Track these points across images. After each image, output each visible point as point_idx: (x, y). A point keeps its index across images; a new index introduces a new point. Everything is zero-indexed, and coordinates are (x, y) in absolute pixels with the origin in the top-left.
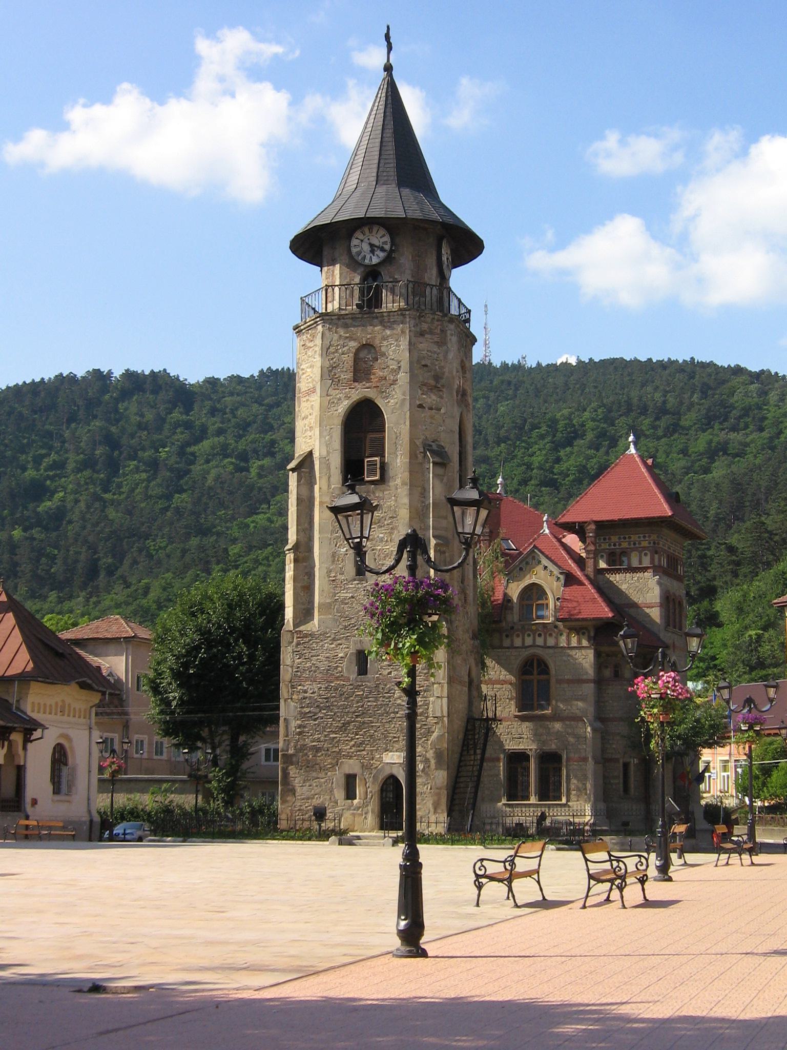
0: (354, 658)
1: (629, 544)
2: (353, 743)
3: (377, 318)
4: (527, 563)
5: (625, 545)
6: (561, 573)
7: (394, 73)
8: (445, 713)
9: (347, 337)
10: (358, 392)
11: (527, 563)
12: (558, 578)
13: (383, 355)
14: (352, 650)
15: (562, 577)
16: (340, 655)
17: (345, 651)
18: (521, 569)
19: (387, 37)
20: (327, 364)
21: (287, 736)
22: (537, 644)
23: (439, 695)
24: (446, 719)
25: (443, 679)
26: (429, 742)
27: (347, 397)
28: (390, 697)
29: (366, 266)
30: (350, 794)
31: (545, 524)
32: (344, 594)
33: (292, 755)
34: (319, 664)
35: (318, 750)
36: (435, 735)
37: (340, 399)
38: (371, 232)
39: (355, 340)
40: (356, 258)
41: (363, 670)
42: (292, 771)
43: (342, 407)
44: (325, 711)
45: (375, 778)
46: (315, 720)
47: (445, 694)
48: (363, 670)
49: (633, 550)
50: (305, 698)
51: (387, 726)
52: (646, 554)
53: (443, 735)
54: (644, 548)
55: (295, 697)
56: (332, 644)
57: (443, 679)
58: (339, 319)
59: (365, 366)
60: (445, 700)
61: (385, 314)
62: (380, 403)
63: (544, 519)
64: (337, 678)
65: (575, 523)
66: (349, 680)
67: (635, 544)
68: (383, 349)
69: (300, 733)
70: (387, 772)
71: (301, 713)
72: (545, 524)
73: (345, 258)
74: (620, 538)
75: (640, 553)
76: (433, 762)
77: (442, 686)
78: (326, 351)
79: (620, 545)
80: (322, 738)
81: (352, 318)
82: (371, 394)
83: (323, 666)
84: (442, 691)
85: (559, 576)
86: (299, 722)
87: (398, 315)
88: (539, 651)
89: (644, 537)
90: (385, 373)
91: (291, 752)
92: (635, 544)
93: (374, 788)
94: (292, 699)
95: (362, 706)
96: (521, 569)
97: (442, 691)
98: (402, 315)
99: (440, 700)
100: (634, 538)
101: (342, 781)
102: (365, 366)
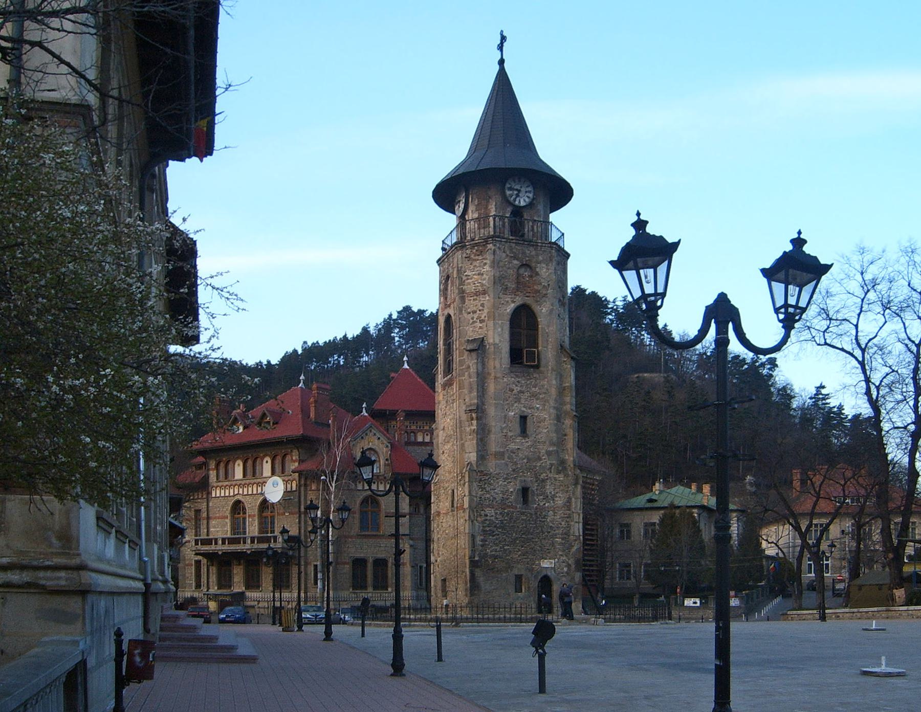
0: (520, 492)
1: (417, 427)
3: (533, 245)
4: (366, 434)
5: (414, 427)
6: (389, 443)
7: (505, 65)
8: (581, 534)
9: (511, 257)
10: (519, 301)
11: (366, 434)
12: (387, 446)
13: (537, 274)
15: (389, 446)
16: (511, 490)
18: (362, 438)
20: (498, 274)
21: (474, 547)
22: (380, 489)
24: (581, 537)
25: (580, 510)
27: (513, 302)
29: (517, 207)
30: (518, 589)
31: (364, 409)
32: (512, 446)
35: (496, 557)
36: (575, 548)
37: (508, 302)
38: (520, 181)
39: (517, 260)
42: (478, 573)
44: (500, 530)
45: (536, 577)
46: (493, 536)
47: (581, 520)
50: (487, 520)
51: (543, 541)
52: (427, 435)
54: (426, 431)
55: (479, 519)
56: (505, 481)
57: (580, 510)
58: (506, 242)
60: (581, 525)
61: (539, 244)
62: (536, 308)
63: (364, 406)
64: (509, 507)
65: (386, 410)
66: (516, 508)
67: (420, 427)
69: (482, 546)
71: (484, 531)
72: (364, 409)
73: (499, 198)
75: (424, 433)
76: (573, 566)
77: (579, 515)
82: (529, 301)
83: (499, 497)
84: (579, 518)
85: (388, 444)
86: (482, 537)
87: (548, 247)
88: (240, 498)
89: (427, 423)
90: (540, 287)
91: (477, 558)
92: (420, 427)
93: (535, 584)
94: (477, 520)
96: (362, 438)
97: (579, 518)
99: (577, 524)
100: (420, 423)
101: (513, 579)
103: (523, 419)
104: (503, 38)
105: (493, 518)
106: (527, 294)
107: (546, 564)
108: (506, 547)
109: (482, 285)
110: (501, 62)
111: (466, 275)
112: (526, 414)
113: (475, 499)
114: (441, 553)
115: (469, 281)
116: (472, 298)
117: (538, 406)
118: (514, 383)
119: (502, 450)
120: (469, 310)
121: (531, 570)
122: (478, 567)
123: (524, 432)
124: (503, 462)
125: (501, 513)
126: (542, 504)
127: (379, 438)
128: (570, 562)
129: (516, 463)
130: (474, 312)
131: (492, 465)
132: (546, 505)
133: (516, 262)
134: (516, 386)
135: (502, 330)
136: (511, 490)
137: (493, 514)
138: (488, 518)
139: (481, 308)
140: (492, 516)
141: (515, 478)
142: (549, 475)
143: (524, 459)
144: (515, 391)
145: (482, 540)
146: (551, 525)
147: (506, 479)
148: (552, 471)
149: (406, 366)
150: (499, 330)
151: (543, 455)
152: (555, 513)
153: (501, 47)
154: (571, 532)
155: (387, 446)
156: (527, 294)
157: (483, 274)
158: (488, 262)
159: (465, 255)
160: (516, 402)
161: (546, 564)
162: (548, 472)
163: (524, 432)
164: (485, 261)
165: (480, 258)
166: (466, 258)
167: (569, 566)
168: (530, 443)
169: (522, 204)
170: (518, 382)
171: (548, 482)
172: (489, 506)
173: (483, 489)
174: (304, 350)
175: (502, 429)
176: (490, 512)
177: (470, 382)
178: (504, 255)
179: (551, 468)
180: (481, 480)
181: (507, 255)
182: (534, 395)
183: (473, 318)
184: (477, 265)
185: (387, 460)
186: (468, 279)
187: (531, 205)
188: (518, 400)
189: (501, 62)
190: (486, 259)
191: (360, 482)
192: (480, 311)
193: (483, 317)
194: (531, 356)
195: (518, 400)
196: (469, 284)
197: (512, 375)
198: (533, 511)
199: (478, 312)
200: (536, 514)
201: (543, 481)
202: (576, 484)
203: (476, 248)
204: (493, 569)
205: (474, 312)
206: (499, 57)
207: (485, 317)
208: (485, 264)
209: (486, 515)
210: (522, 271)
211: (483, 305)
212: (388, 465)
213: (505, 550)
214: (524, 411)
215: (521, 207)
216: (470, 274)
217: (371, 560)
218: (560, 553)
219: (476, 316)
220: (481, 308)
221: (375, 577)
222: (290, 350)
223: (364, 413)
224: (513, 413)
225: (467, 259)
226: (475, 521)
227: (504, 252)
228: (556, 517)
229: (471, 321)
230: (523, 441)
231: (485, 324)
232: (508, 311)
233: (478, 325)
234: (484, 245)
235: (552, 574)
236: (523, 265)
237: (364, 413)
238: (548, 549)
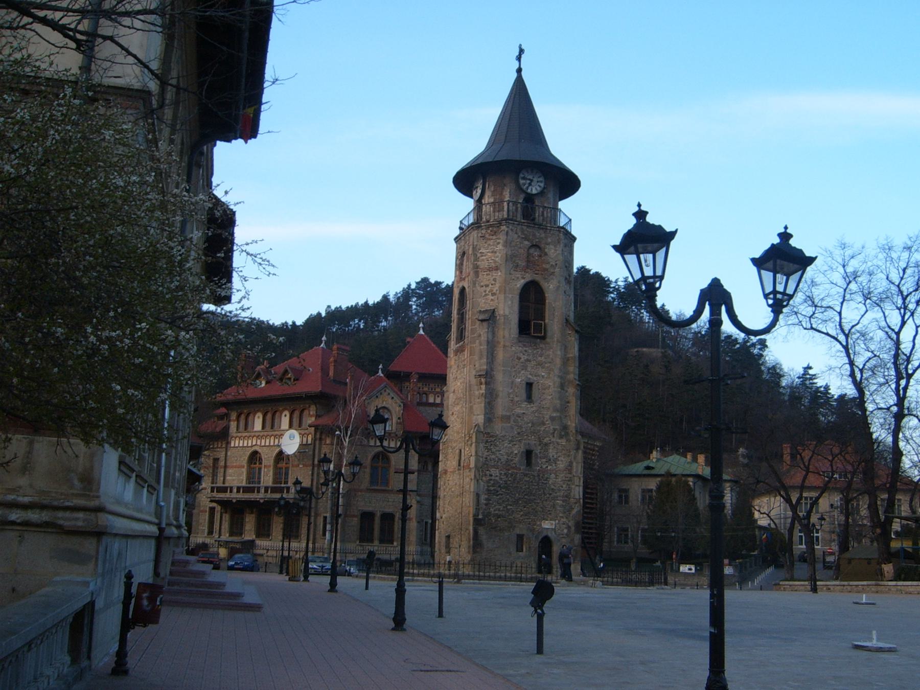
0: (524, 455)
1: (429, 389)
2: (522, 513)
3: (543, 229)
5: (426, 389)
6: (402, 402)
7: (523, 73)
8: (581, 497)
9: (523, 238)
10: (529, 277)
11: (381, 394)
13: (546, 254)
14: (523, 449)
15: (402, 405)
17: (518, 449)
18: (377, 397)
19: (273, 67)
20: (510, 253)
23: (578, 484)
24: (581, 500)
26: (571, 515)
27: (524, 278)
28: (546, 483)
30: (519, 549)
33: (481, 520)
34: (501, 457)
35: (499, 516)
37: (518, 278)
40: (522, 186)
41: (529, 463)
43: (520, 283)
45: (537, 537)
46: (497, 495)
48: (529, 463)
49: (431, 393)
50: (491, 480)
51: (544, 502)
52: (438, 396)
53: (579, 511)
55: (484, 478)
58: (518, 225)
59: (532, 259)
60: (581, 488)
62: (544, 285)
64: (513, 468)
66: (520, 469)
67: (432, 389)
68: (546, 250)
69: (486, 505)
70: (544, 534)
74: (423, 385)
76: (573, 528)
78: (507, 244)
79: (423, 388)
80: (501, 509)
81: (527, 226)
82: (538, 278)
84: (580, 481)
85: (401, 404)
86: (486, 496)
90: (547, 266)
91: (480, 517)
92: (432, 389)
93: (535, 544)
95: (529, 488)
97: (580, 481)
98: (559, 231)
100: (431, 386)
101: (514, 539)
102: (532, 259)
103: (529, 385)
104: (521, 51)
105: (497, 478)
106: (536, 272)
107: (547, 525)
108: (509, 507)
109: (495, 262)
110: (519, 71)
111: (481, 253)
112: (531, 381)
113: (481, 459)
114: (446, 510)
115: (483, 258)
116: (485, 273)
117: (543, 374)
118: (521, 352)
119: (508, 414)
120: (482, 284)
121: (533, 530)
122: (481, 525)
123: (529, 398)
124: (509, 425)
125: (505, 474)
126: (544, 467)
127: (393, 398)
128: (570, 524)
129: (521, 427)
130: (487, 286)
131: (498, 428)
132: (549, 468)
133: (526, 243)
134: (524, 354)
135: (512, 303)
136: (516, 452)
137: (498, 474)
138: (493, 478)
139: (493, 282)
140: (497, 476)
141: (520, 441)
142: (552, 440)
143: (529, 423)
144: (522, 360)
145: (486, 499)
146: (552, 487)
147: (511, 441)
148: (555, 436)
149: (421, 332)
150: (510, 302)
151: (547, 421)
152: (556, 476)
153: (519, 58)
154: (572, 494)
155: (400, 406)
156: (536, 272)
157: (496, 252)
158: (501, 241)
159: (480, 235)
160: (523, 369)
161: (547, 525)
162: (551, 436)
163: (529, 398)
164: (498, 241)
165: (494, 237)
166: (481, 237)
167: (569, 528)
168: (534, 409)
169: (534, 192)
170: (526, 351)
171: (551, 447)
172: (493, 466)
173: (489, 450)
174: (328, 313)
175: (509, 394)
176: (495, 472)
177: (480, 349)
178: (516, 236)
179: (554, 433)
180: (487, 442)
181: (519, 236)
182: (540, 364)
183: (485, 291)
184: (491, 244)
185: (399, 418)
186: (482, 256)
187: (542, 193)
188: (525, 368)
189: (519, 71)
190: (500, 239)
191: (372, 439)
192: (492, 285)
193: (494, 291)
194: (538, 328)
195: (525, 368)
196: (483, 260)
197: (520, 344)
198: (535, 474)
199: (490, 286)
200: (539, 476)
201: (546, 445)
202: (577, 449)
203: (491, 228)
204: (495, 528)
205: (487, 286)
206: (517, 66)
207: (497, 290)
208: (499, 243)
209: (491, 475)
210: (532, 251)
211: (495, 280)
212: (400, 423)
213: (508, 510)
214: (530, 379)
215: (532, 194)
216: (484, 251)
217: (378, 514)
218: (561, 515)
219: (488, 289)
220: (493, 282)
221: (382, 530)
222: (315, 313)
223: (380, 373)
224: (519, 380)
225: (482, 238)
226: (480, 481)
227: (516, 233)
228: (557, 480)
229: (484, 294)
230: (529, 406)
231: (496, 297)
232: (518, 286)
233: (490, 297)
234: (498, 227)
235: (552, 535)
236: (533, 246)
237: (380, 373)
238: (549, 511)
